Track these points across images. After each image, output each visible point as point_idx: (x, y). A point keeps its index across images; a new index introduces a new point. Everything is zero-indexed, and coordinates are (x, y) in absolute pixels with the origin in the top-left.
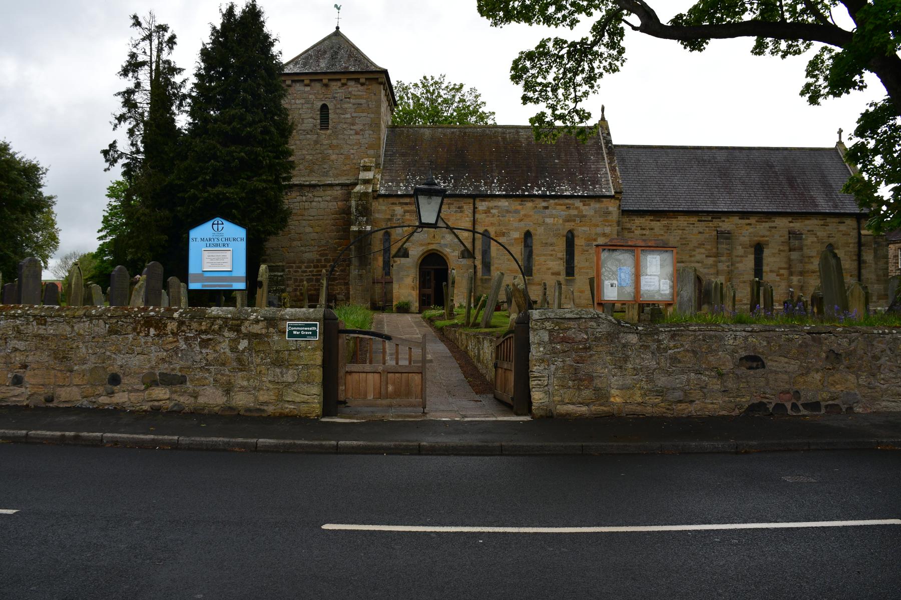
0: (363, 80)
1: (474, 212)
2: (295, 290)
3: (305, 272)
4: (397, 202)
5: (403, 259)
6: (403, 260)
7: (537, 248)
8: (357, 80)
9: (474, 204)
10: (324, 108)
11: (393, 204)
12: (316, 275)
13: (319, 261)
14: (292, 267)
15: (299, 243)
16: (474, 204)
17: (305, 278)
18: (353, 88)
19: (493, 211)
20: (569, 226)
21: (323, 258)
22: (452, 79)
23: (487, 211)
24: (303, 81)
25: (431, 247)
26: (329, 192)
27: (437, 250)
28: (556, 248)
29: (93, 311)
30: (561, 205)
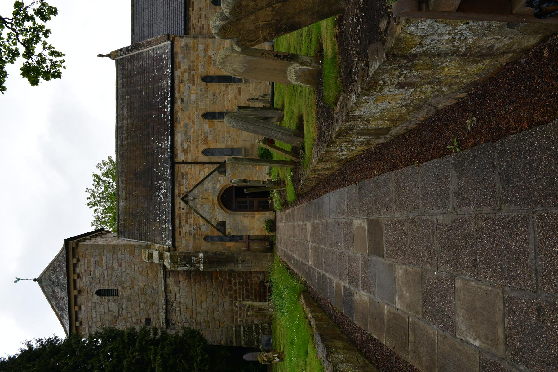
1: (187, 163)
8: (75, 265)
9: (180, 163)
10: (100, 293)
11: (180, 234)
13: (231, 296)
14: (236, 319)
15: (216, 313)
16: (180, 163)
23: (186, 151)
24: (76, 312)
25: (216, 201)
27: (219, 195)
28: (217, 91)
30: (180, 87)
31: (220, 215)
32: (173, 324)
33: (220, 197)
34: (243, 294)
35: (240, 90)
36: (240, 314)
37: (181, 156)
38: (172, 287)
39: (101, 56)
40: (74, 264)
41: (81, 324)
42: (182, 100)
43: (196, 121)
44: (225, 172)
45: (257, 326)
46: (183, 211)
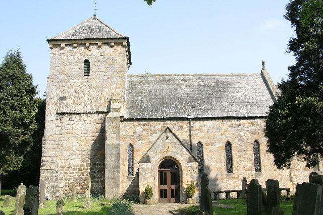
0: (75, 45)
1: (190, 130)
2: (65, 186)
3: (73, 173)
4: (137, 124)
5: (145, 164)
6: (148, 165)
7: (234, 153)
8: (108, 44)
9: (190, 124)
10: (87, 62)
11: (134, 125)
12: (80, 175)
13: (82, 165)
14: (63, 170)
15: (68, 153)
16: (190, 124)
17: (72, 178)
18: (106, 49)
19: (204, 129)
20: (255, 137)
21: (85, 164)
22: (287, 46)
23: (200, 129)
24: (72, 44)
25: (168, 154)
26: (89, 118)
27: (171, 157)
28: (247, 152)
29: (284, 153)
30: (249, 123)
31: (156, 159)
32: (60, 119)
33: (170, 158)
34: (83, 175)
35: (250, 170)
36: (67, 173)
37: (196, 125)
38: (90, 118)
39: (263, 63)
40: (122, 43)
41: (88, 47)
42: (239, 125)
43: (223, 137)
44: (191, 162)
45: (57, 186)
46: (152, 128)
